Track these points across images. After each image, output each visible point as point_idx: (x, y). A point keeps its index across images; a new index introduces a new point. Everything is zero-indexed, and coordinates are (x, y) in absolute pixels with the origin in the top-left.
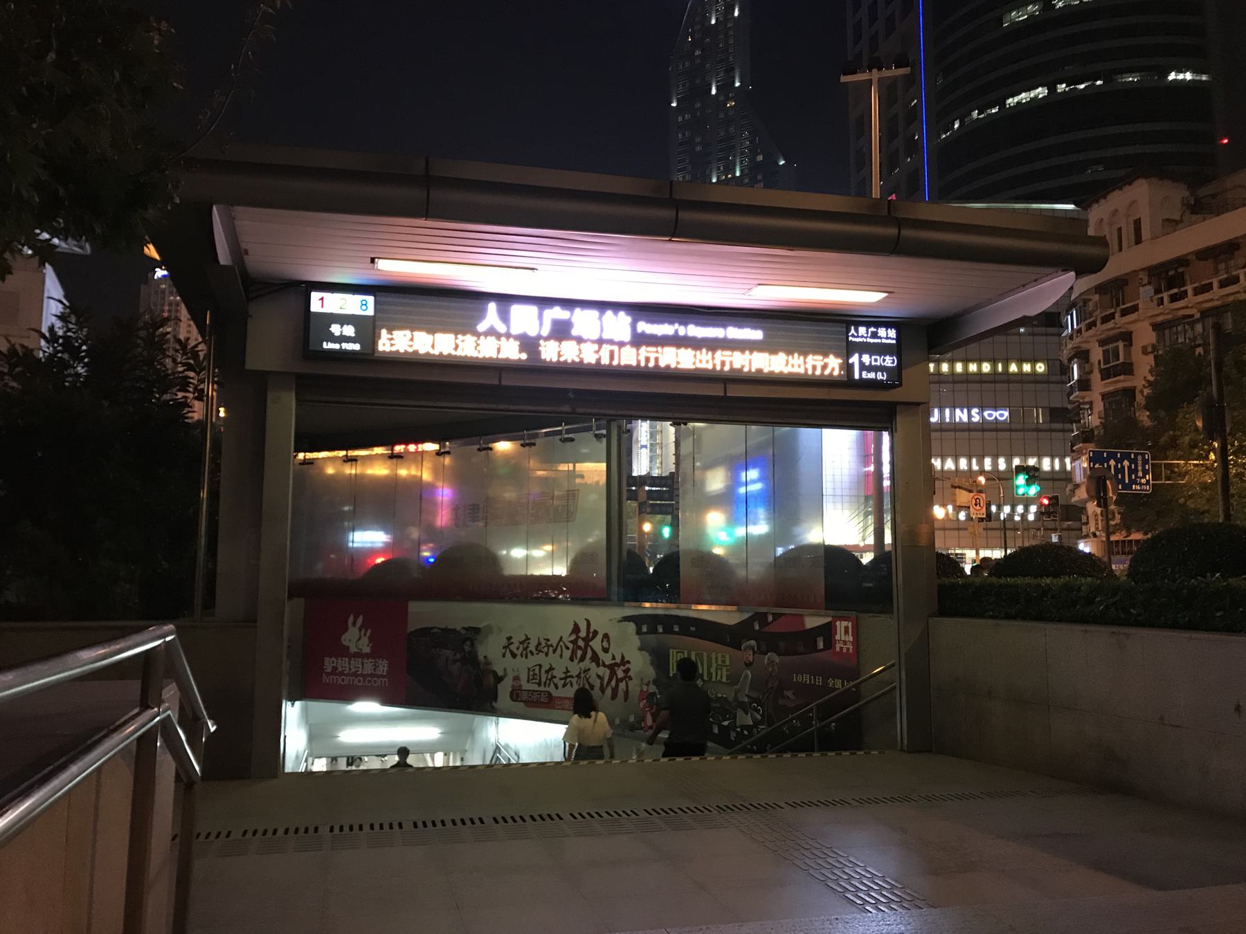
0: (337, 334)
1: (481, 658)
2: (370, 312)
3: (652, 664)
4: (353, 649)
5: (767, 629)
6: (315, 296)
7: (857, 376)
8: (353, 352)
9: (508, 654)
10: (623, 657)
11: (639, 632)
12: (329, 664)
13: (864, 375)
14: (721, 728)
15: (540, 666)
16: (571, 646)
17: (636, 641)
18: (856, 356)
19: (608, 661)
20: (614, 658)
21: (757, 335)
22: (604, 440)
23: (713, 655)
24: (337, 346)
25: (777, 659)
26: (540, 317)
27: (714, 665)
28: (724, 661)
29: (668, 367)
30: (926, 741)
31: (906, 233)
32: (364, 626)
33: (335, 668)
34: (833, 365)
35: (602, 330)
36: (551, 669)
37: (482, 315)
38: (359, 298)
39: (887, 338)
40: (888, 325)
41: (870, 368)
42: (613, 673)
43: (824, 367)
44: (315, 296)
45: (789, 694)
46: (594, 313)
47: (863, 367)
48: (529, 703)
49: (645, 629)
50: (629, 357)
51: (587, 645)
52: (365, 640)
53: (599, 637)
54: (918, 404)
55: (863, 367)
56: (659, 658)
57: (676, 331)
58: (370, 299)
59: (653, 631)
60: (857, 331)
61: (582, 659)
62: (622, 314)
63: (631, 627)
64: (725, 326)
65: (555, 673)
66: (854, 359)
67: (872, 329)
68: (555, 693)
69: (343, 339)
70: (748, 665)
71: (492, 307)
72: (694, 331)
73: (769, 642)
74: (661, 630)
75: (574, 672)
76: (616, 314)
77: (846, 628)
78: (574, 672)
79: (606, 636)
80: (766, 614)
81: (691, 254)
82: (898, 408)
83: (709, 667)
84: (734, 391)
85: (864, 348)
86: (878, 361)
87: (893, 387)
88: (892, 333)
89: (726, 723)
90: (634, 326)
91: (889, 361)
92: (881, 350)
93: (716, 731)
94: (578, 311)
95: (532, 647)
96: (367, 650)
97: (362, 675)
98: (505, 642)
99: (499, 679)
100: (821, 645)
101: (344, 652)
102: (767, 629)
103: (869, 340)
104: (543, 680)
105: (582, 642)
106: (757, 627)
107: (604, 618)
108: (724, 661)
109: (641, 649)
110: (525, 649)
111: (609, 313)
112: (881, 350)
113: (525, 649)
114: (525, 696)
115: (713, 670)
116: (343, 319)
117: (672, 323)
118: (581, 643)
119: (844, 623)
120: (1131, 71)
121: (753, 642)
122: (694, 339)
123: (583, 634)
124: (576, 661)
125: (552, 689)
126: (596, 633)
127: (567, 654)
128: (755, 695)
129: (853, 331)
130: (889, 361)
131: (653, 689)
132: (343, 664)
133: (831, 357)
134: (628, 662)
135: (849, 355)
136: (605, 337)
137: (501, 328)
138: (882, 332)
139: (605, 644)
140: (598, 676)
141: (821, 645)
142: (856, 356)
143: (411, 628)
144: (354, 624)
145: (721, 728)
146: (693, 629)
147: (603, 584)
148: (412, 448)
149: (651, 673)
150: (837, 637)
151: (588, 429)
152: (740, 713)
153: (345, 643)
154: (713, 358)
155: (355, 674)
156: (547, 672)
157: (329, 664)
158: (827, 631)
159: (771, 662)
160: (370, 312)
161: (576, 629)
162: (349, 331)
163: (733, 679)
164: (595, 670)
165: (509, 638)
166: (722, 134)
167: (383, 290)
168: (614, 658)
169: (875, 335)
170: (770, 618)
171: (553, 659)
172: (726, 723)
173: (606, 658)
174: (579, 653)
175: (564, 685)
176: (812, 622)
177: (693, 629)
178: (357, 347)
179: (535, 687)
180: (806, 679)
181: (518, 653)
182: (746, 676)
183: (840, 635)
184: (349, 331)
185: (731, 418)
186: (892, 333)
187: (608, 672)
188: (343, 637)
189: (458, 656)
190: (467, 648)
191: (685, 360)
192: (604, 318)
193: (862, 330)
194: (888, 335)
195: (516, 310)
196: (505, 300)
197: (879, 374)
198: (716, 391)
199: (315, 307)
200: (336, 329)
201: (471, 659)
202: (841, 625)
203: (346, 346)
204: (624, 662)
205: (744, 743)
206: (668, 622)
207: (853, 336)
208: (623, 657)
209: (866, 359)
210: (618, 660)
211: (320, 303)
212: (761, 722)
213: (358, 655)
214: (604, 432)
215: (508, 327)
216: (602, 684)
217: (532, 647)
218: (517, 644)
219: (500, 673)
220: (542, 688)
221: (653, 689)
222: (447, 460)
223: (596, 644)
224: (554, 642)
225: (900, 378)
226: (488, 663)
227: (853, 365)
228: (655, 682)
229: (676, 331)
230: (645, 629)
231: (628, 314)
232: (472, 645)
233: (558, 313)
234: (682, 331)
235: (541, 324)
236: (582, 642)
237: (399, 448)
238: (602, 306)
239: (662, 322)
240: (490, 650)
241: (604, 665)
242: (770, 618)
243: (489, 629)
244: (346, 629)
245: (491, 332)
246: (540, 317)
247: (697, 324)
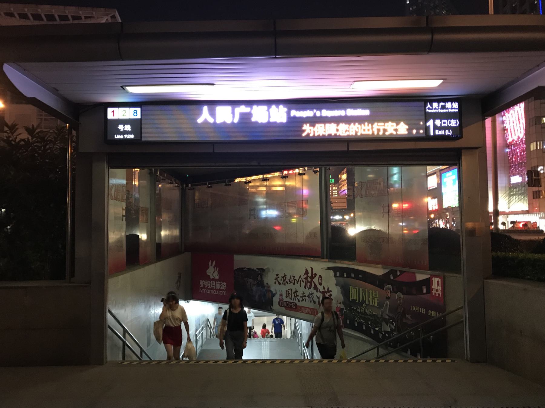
0: (122, 130)
1: (265, 284)
2: (139, 117)
3: (342, 293)
4: (212, 277)
5: (397, 279)
6: (110, 110)
7: (432, 134)
8: (130, 140)
9: (277, 282)
10: (328, 289)
11: (335, 276)
12: (202, 283)
13: (437, 132)
14: (375, 331)
15: (291, 290)
16: (304, 280)
17: (333, 281)
18: (431, 121)
19: (322, 290)
20: (324, 289)
21: (366, 112)
22: (318, 173)
23: (371, 292)
24: (122, 137)
25: (402, 296)
26: (233, 113)
27: (371, 297)
28: (376, 295)
29: (319, 136)
30: (483, 355)
31: (437, 37)
32: (216, 266)
33: (204, 286)
35: (269, 117)
36: (296, 291)
37: (200, 114)
38: (132, 109)
39: (452, 108)
40: (452, 100)
41: (440, 128)
42: (324, 295)
43: (385, 130)
44: (110, 110)
45: (408, 316)
46: (264, 108)
47: (435, 127)
48: (287, 308)
49: (338, 275)
51: (312, 281)
52: (216, 273)
53: (317, 277)
54: (476, 148)
55: (435, 127)
56: (345, 291)
57: (315, 114)
58: (139, 110)
59: (342, 276)
60: (431, 105)
61: (310, 288)
62: (281, 107)
63: (332, 273)
64: (345, 109)
65: (298, 294)
66: (430, 123)
68: (298, 304)
69: (125, 132)
70: (388, 298)
71: (205, 108)
72: (325, 113)
73: (398, 287)
74: (345, 276)
75: (307, 294)
76: (278, 107)
77: (438, 282)
78: (307, 294)
79: (320, 277)
80: (396, 271)
81: (298, 65)
82: (463, 151)
83: (369, 297)
84: (353, 148)
85: (436, 116)
86: (446, 123)
87: (457, 139)
88: (456, 105)
89: (377, 329)
90: (288, 113)
91: (454, 123)
92: (449, 116)
93: (373, 332)
94: (255, 107)
95: (287, 280)
96: (217, 277)
97: (215, 289)
98: (275, 277)
99: (274, 295)
100: (425, 291)
101: (208, 278)
102: (397, 279)
103: (440, 111)
104: (293, 297)
105: (310, 278)
106: (392, 278)
107: (319, 267)
108: (376, 295)
109: (336, 285)
110: (284, 280)
111: (274, 107)
112: (449, 116)
113: (284, 280)
114: (285, 304)
115: (370, 299)
116: (124, 122)
117: (311, 109)
118: (309, 279)
119: (437, 279)
121: (390, 286)
122: (326, 117)
123: (310, 275)
124: (307, 288)
125: (297, 301)
126: (316, 275)
127: (303, 284)
128: (391, 315)
129: (429, 106)
130: (454, 123)
131: (342, 306)
132: (207, 283)
133: (402, 123)
134: (331, 291)
135: (426, 121)
138: (448, 105)
139: (320, 281)
140: (318, 297)
141: (425, 291)
142: (431, 121)
143: (235, 268)
144: (212, 265)
145: (375, 331)
146: (360, 276)
147: (319, 248)
148: (291, 172)
149: (341, 298)
150: (433, 287)
151: (206, 184)
152: (384, 324)
153: (208, 274)
154: (372, 128)
155: (212, 289)
156: (294, 293)
157: (202, 283)
158: (428, 283)
159: (399, 298)
160: (139, 117)
161: (307, 272)
162: (128, 128)
163: (381, 305)
164: (316, 294)
165: (277, 275)
166: (432, 5)
167: (141, 103)
168: (324, 289)
169: (443, 107)
170: (399, 273)
171: (297, 286)
172: (377, 329)
173: (320, 288)
174: (309, 284)
175: (302, 300)
176: (420, 277)
177: (360, 276)
179: (289, 300)
180: (416, 309)
181: (281, 282)
182: (387, 304)
183: (434, 286)
184: (128, 128)
186: (456, 105)
187: (322, 295)
188: (207, 271)
189: (256, 282)
190: (259, 279)
192: (271, 110)
193: (435, 105)
194: (453, 107)
195: (219, 109)
196: (212, 104)
197: (447, 131)
198: (343, 148)
199: (110, 116)
200: (121, 127)
201: (261, 284)
202: (435, 280)
204: (329, 291)
205: (386, 341)
206: (349, 271)
207: (429, 109)
208: (328, 289)
209: (438, 122)
210: (326, 290)
211: (113, 114)
212: (394, 330)
213: (214, 280)
214: (318, 169)
215: (215, 118)
216: (319, 302)
217: (287, 280)
218: (280, 278)
219: (274, 292)
220: (292, 301)
221: (342, 306)
222: (305, 177)
223: (316, 280)
224: (297, 278)
225: (461, 134)
226: (269, 287)
227: (429, 126)
228: (344, 303)
229: (315, 114)
230: (338, 275)
231: (284, 107)
232: (261, 277)
233: (243, 109)
234: (318, 114)
235: (234, 117)
236: (310, 278)
237: (285, 172)
238: (269, 103)
240: (269, 279)
241: (320, 292)
242: (399, 273)
243: (268, 270)
244: (208, 268)
246: (233, 113)
247: (327, 109)
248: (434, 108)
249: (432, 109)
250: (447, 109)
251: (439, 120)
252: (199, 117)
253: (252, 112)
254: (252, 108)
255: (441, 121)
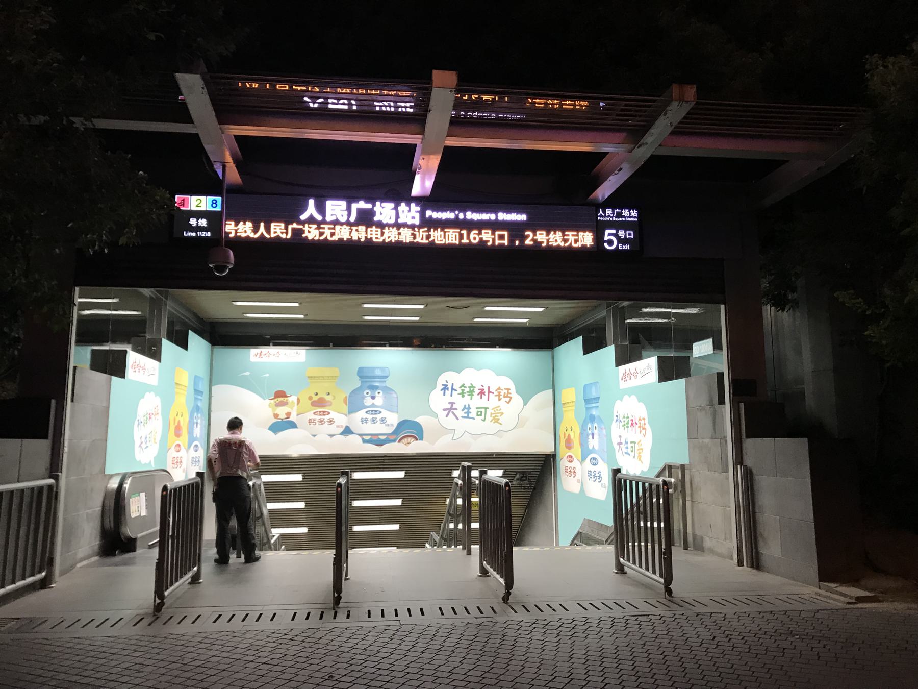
0: (195, 225)
8: (206, 238)
26: (349, 209)
34: (586, 239)
39: (630, 217)
50: (421, 237)
57: (457, 216)
60: (604, 212)
67: (362, 205)
69: (198, 229)
90: (422, 214)
91: (630, 234)
116: (199, 215)
117: (453, 210)
120: (255, 81)
136: (400, 221)
137: (319, 218)
154: (366, 231)
160: (218, 209)
162: (203, 223)
169: (366, 218)
178: (209, 234)
184: (203, 223)
185: (297, 286)
191: (451, 237)
192: (399, 208)
193: (609, 211)
200: (193, 222)
203: (204, 234)
207: (601, 216)
229: (457, 216)
235: (349, 215)
239: (446, 211)
245: (311, 220)
246: (349, 209)
248: (329, 218)
249: (605, 216)
250: (624, 217)
251: (364, 228)
252: (303, 213)
253: (375, 209)
254: (374, 205)
255: (493, 234)
